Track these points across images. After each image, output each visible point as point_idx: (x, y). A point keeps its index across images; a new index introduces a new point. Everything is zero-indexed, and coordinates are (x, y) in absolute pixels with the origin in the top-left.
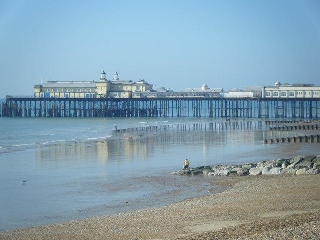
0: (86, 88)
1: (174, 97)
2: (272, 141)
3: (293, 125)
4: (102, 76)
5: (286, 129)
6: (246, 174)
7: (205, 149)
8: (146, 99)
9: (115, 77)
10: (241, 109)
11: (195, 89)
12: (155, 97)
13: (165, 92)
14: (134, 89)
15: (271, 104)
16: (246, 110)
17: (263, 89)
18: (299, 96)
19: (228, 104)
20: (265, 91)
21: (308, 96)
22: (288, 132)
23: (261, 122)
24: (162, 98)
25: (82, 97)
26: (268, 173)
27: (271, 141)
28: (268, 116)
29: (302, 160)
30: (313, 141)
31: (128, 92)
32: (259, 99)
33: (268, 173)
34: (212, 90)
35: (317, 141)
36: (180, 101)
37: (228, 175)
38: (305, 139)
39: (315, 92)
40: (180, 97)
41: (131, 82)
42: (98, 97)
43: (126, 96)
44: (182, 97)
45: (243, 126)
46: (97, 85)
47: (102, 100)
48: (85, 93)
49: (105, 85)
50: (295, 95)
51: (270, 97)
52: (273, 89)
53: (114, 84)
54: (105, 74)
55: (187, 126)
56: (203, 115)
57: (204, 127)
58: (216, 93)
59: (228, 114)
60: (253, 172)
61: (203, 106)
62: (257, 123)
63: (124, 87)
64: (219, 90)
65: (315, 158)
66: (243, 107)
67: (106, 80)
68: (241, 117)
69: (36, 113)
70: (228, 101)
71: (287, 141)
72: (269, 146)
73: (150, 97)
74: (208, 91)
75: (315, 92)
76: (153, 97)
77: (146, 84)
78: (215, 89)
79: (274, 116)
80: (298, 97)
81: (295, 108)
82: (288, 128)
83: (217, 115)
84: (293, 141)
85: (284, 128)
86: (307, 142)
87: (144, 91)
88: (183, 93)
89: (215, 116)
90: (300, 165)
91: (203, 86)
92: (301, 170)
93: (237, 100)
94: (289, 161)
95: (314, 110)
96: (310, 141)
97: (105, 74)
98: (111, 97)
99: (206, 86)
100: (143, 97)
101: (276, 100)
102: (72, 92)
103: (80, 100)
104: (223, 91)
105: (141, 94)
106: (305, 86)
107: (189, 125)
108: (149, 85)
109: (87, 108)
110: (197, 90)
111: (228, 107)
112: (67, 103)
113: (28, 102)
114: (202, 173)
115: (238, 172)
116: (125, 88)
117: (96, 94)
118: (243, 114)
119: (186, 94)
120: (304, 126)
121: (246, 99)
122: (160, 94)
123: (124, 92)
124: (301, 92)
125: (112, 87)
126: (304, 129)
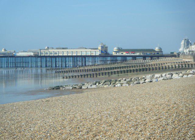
2: (67, 77)
6: (81, 88)
7: (4, 84)
16: (28, 63)
17: (39, 51)
20: (40, 52)
21: (65, 54)
23: (32, 70)
26: (91, 87)
29: (105, 82)
30: (87, 77)
32: (36, 56)
34: (8, 51)
37: (72, 89)
38: (84, 76)
51: (44, 55)
56: (3, 66)
57: (3, 72)
58: (11, 53)
60: (83, 87)
62: (35, 69)
64: (12, 51)
65: (111, 80)
66: (13, 62)
70: (23, 58)
72: (65, 80)
74: (6, 52)
84: (78, 77)
86: (87, 77)
89: (11, 66)
90: (105, 83)
92: (106, 86)
93: (24, 57)
95: (67, 62)
99: (5, 49)
104: (15, 52)
106: (63, 49)
114: (59, 88)
115: (77, 87)
117: (162, 54)
121: (29, 56)
124: (75, 52)
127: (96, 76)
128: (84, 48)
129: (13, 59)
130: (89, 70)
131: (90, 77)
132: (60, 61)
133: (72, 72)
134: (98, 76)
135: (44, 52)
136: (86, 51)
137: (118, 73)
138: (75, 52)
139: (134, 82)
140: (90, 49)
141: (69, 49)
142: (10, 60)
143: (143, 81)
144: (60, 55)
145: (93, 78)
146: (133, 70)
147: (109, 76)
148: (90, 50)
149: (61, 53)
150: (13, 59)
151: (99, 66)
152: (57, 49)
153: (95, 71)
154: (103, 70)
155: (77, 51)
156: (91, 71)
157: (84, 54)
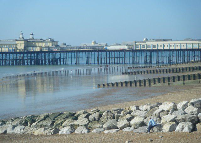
0: (9, 44)
1: (72, 50)
2: (104, 85)
3: (145, 69)
4: (21, 36)
5: (134, 74)
8: (52, 52)
9: (31, 36)
10: (120, 58)
11: (87, 44)
12: (58, 50)
13: (65, 46)
14: (44, 45)
15: (140, 54)
17: (134, 43)
18: (160, 48)
19: (111, 54)
20: (135, 44)
21: (166, 48)
22: (135, 76)
24: (63, 51)
25: (6, 51)
27: (102, 85)
28: (139, 62)
30: (136, 85)
31: (39, 47)
32: (131, 50)
33: (12, 131)
34: (98, 45)
35: (139, 85)
36: (66, 53)
38: (129, 83)
39: (177, 45)
40: (76, 50)
41: (42, 39)
42: (18, 51)
43: (38, 49)
44: (77, 50)
45: (114, 71)
46: (17, 42)
47: (20, 53)
48: (9, 48)
49: (23, 42)
50: (157, 47)
51: (139, 49)
52: (142, 43)
53: (29, 42)
54: (22, 34)
55: (82, 70)
56: (93, 62)
58: (101, 47)
59: (111, 62)
61: (93, 57)
63: (36, 44)
64: (103, 44)
67: (23, 38)
68: (120, 63)
69: (27, 62)
70: (111, 52)
71: (115, 85)
73: (54, 50)
75: (177, 45)
76: (57, 50)
77: (52, 41)
78: (101, 43)
79: (143, 62)
80: (176, 48)
81: (158, 56)
82: (135, 72)
83: (113, 62)
85: (132, 73)
86: (131, 85)
87: (51, 46)
88: (78, 47)
90: (41, 123)
91: (93, 42)
93: (117, 51)
94: (33, 118)
96: (133, 85)
97: (22, 34)
98: (27, 50)
99: (95, 42)
100: (50, 50)
101: (144, 50)
102: (6, 48)
103: (6, 53)
104: (106, 45)
105: (49, 48)
106: (164, 40)
107: (83, 70)
108: (54, 42)
109: (51, 58)
110: (88, 45)
111: (111, 56)
112: (25, 55)
113: (7, 55)
116: (37, 44)
117: (17, 49)
118: (121, 61)
119: (80, 48)
120: (163, 70)
121: (123, 51)
122: (62, 48)
123: (37, 47)
124: (161, 45)
125: (28, 43)
126: (144, 73)
127: (148, 84)
128: (190, 39)
129: (86, 54)
130: (168, 70)
131: (140, 85)
132: (175, 55)
133: (144, 73)
134: (152, 84)
135: (140, 45)
136: (192, 44)
137: (184, 80)
138: (178, 45)
139: (103, 124)
140: (197, 40)
141: (174, 41)
142: (136, 55)
143: (125, 122)
144: (160, 48)
145: (143, 87)
146: (193, 75)
147: (169, 84)
148: (198, 42)
149: (161, 45)
150: (86, 54)
151: (196, 63)
152: (157, 41)
153: (177, 71)
154: (188, 70)
155: (181, 44)
156: (171, 72)
157: (190, 47)
